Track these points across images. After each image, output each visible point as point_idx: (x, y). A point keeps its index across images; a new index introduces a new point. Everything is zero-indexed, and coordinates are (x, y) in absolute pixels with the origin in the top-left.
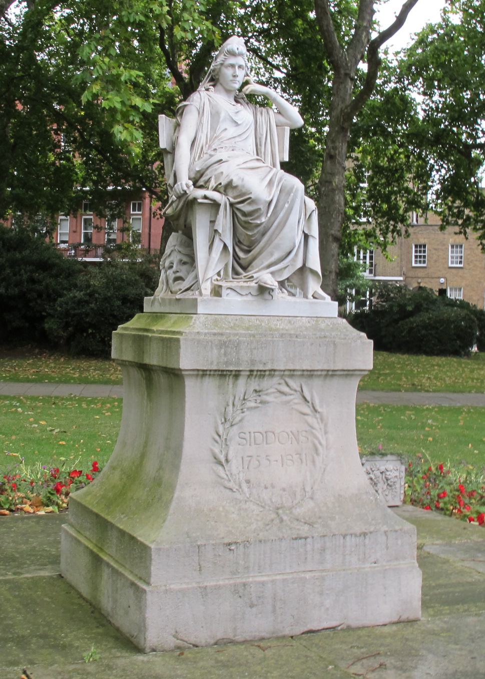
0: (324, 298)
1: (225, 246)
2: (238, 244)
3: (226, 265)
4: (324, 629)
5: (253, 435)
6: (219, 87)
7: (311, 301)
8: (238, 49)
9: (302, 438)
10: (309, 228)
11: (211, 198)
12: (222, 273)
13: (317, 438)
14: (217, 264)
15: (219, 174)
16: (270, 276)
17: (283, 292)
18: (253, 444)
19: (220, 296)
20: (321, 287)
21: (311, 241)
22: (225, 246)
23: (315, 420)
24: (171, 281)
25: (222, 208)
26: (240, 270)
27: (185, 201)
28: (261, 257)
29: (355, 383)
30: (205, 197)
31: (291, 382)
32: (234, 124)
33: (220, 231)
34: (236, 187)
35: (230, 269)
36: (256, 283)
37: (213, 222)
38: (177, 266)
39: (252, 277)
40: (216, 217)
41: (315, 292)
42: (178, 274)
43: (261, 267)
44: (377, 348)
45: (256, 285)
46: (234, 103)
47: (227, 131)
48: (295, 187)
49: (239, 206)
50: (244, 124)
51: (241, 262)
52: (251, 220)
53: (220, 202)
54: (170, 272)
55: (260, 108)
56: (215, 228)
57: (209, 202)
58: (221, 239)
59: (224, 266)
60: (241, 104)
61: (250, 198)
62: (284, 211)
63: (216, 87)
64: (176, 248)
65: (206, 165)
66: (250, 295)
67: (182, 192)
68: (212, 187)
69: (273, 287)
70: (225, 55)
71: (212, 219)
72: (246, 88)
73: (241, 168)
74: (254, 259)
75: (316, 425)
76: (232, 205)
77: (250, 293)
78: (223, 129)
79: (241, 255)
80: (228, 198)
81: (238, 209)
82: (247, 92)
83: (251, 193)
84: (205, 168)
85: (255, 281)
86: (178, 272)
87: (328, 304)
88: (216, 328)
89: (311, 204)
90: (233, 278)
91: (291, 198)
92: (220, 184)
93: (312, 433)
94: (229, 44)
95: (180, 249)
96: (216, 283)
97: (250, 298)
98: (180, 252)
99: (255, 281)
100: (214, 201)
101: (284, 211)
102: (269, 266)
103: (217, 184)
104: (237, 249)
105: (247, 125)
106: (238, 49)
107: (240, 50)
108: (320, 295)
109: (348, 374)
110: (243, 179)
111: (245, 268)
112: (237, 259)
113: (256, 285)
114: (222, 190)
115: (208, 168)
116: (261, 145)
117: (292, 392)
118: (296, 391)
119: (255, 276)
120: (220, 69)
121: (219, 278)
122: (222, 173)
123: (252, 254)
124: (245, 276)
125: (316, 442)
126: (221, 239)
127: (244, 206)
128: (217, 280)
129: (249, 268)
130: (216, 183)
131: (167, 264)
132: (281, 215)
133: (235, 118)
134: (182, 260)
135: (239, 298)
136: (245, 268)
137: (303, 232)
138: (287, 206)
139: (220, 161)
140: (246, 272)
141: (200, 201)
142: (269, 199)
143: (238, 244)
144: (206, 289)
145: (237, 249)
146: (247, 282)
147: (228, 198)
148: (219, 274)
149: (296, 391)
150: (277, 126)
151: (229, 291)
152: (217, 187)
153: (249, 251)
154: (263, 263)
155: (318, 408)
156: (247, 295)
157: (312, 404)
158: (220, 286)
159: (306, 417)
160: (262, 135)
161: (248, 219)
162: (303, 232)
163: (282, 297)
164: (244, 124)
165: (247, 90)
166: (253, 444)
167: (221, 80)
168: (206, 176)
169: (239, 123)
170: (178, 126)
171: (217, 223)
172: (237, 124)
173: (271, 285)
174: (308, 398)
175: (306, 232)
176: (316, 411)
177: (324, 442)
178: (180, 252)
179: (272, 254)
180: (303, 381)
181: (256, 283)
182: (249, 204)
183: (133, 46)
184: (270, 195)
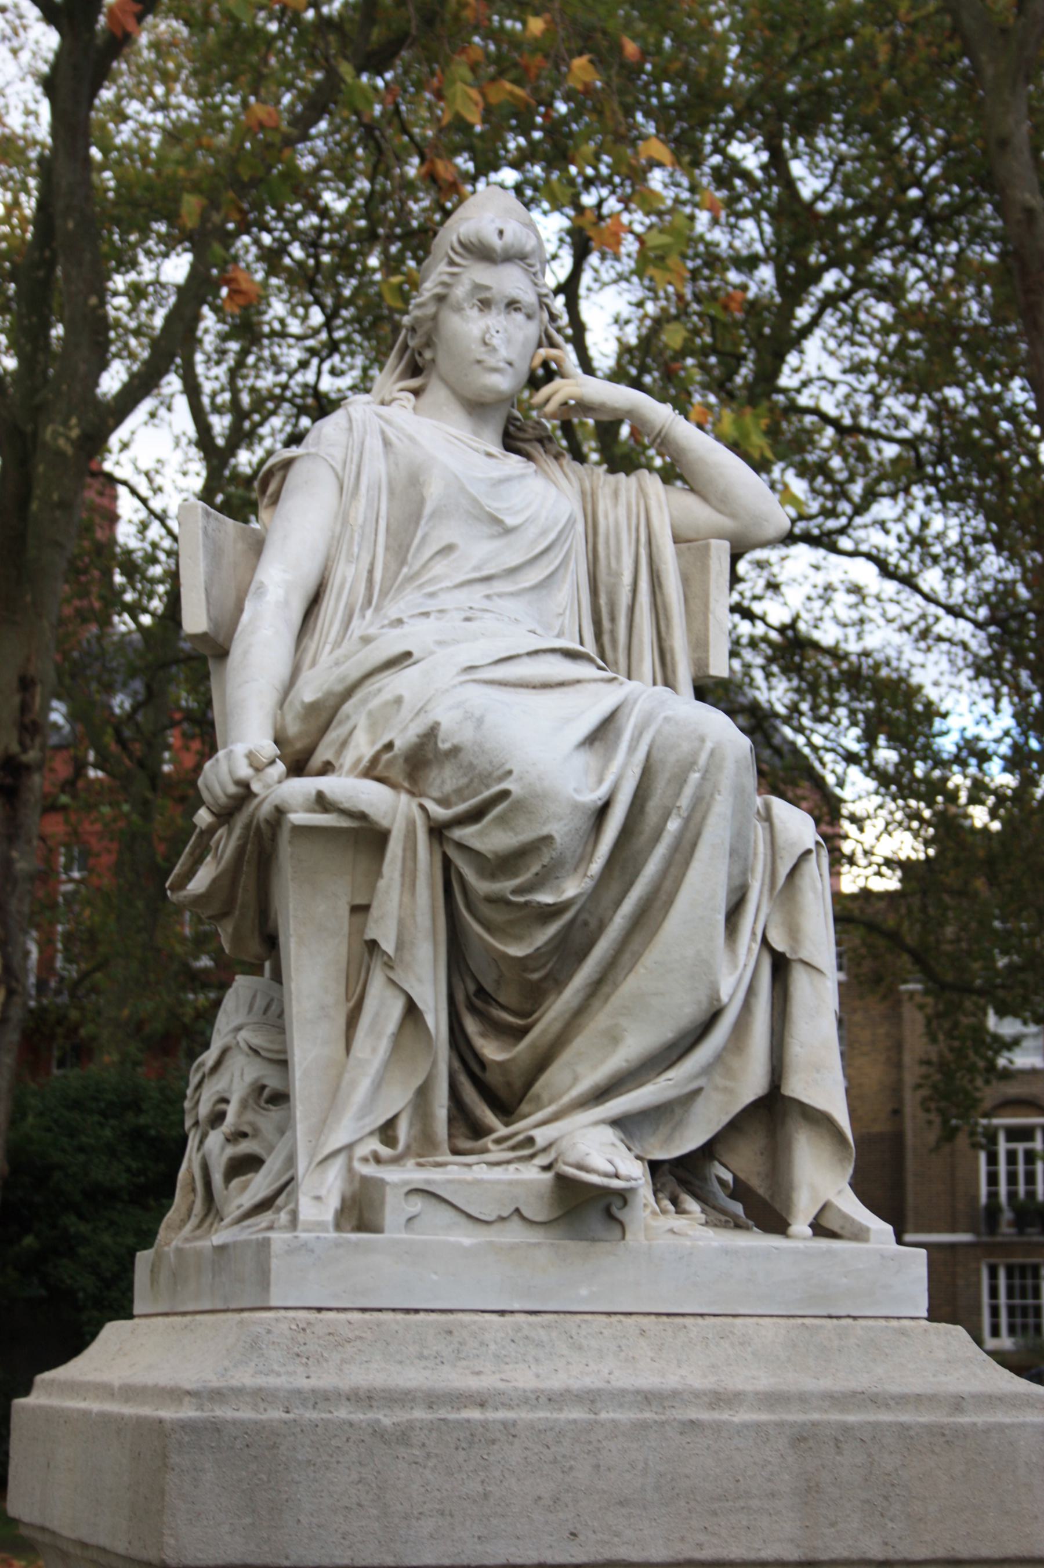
0: (860, 1234)
1: (412, 1010)
2: (478, 1003)
3: (423, 1093)
6: (437, 393)
7: (800, 1244)
8: (501, 233)
10: (793, 932)
11: (346, 805)
12: (403, 1131)
14: (378, 1085)
15: (386, 704)
16: (610, 1134)
17: (680, 1211)
19: (377, 1229)
20: (851, 1185)
21: (800, 982)
22: (412, 1010)
24: (217, 1178)
25: (395, 848)
26: (489, 1117)
27: (247, 827)
28: (566, 1056)
30: (322, 802)
33: (388, 946)
34: (455, 751)
35: (441, 1110)
36: (547, 1168)
37: (360, 910)
38: (240, 1114)
39: (530, 1141)
40: (372, 888)
41: (825, 1207)
42: (245, 1147)
43: (566, 1099)
44: (125, 1312)
45: (548, 1176)
46: (497, 450)
47: (454, 556)
48: (709, 745)
49: (464, 834)
50: (532, 531)
51: (492, 1078)
52: (514, 892)
53: (385, 823)
54: (215, 1138)
55: (612, 478)
56: (370, 935)
57: (344, 823)
58: (392, 982)
59: (409, 1094)
60: (529, 457)
61: (505, 794)
62: (661, 850)
63: (427, 398)
64: (243, 1035)
65: (341, 680)
66: (516, 1223)
67: (232, 789)
68: (359, 760)
69: (633, 1184)
70: (452, 263)
71: (360, 901)
73: (475, 681)
74: (543, 1061)
76: (438, 831)
77: (517, 1210)
78: (443, 544)
79: (492, 1051)
80: (422, 807)
81: (461, 847)
83: (510, 773)
84: (339, 688)
85: (542, 1160)
86: (244, 1135)
90: (455, 1152)
91: (688, 791)
92: (389, 746)
94: (467, 219)
95: (257, 1041)
96: (369, 1170)
97: (515, 1234)
98: (256, 1052)
99: (542, 1160)
100: (362, 816)
101: (661, 850)
102: (601, 1094)
103: (378, 746)
104: (471, 1026)
105: (544, 533)
106: (501, 233)
107: (508, 236)
108: (845, 1217)
110: (480, 722)
111: (507, 1110)
112: (476, 1068)
113: (548, 1176)
114: (397, 774)
115: (349, 693)
116: (613, 619)
119: (542, 1135)
120: (434, 318)
121: (385, 1151)
122: (398, 701)
123: (533, 1046)
124: (498, 1141)
126: (392, 982)
127: (481, 834)
128: (378, 1159)
129: (524, 1108)
130: (373, 743)
131: (204, 1110)
132: (652, 868)
133: (492, 505)
134: (263, 1087)
135: (466, 1237)
136: (507, 1110)
137: (765, 942)
138: (673, 825)
139: (403, 659)
140: (507, 1124)
141: (298, 818)
142: (594, 796)
143: (478, 1003)
144: (318, 1198)
145: (471, 1026)
146: (508, 1162)
147: (422, 807)
148: (387, 1132)
150: (677, 540)
151: (417, 1205)
152: (375, 760)
153: (522, 1032)
154: (576, 1080)
156: (502, 1219)
158: (381, 1183)
160: (618, 575)
161: (505, 886)
162: (765, 942)
163: (672, 1231)
164: (532, 531)
165: (547, 400)
167: (444, 364)
168: (340, 723)
169: (510, 521)
170: (257, 546)
171: (374, 912)
172: (501, 529)
173: (607, 1175)
175: (779, 944)
178: (256, 1052)
179: (613, 1038)
181: (547, 1168)
182: (502, 821)
184: (600, 781)
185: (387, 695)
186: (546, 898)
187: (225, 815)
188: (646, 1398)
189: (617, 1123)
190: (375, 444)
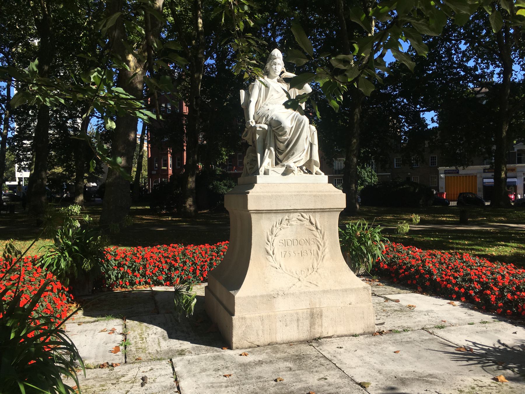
4: (324, 337)
5: (286, 241)
9: (312, 242)
13: (319, 242)
18: (286, 245)
23: (317, 233)
29: (337, 215)
30: (260, 127)
31: (304, 214)
32: (277, 92)
72: (283, 74)
75: (318, 236)
82: (283, 77)
87: (323, 177)
88: (103, 21)
89: (313, 128)
93: (316, 239)
109: (331, 210)
111: (281, 161)
117: (306, 220)
118: (307, 219)
125: (319, 244)
149: (307, 219)
155: (319, 227)
157: (316, 225)
159: (313, 232)
166: (286, 245)
174: (314, 223)
176: (423, 329)
177: (322, 244)
180: (311, 214)
183: (413, 39)
186: (286, 138)
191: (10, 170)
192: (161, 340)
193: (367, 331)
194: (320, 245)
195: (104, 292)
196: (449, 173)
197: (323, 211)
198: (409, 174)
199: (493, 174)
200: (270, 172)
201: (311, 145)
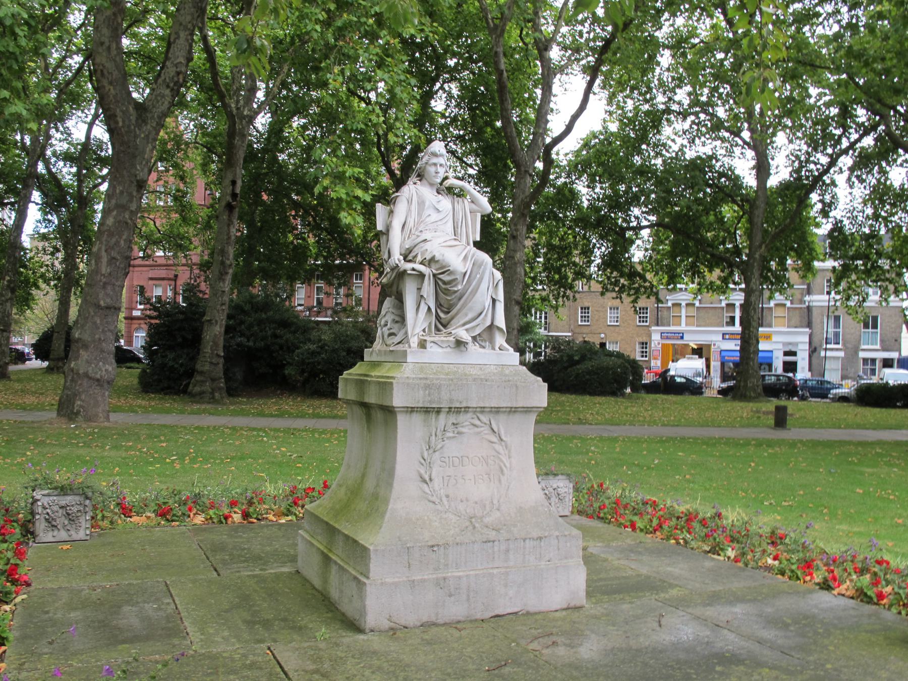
0: (508, 350)
1: (429, 309)
3: (430, 324)
6: (424, 181)
9: (490, 462)
10: (496, 294)
13: (502, 462)
21: (498, 304)
22: (429, 309)
24: (386, 336)
25: (426, 278)
29: (533, 417)
30: (413, 269)
31: (482, 417)
34: (438, 261)
37: (419, 289)
42: (391, 331)
47: (787, 349)
49: (440, 276)
51: (442, 321)
74: (452, 318)
75: (501, 451)
76: (434, 275)
79: (442, 315)
81: (440, 279)
97: (449, 350)
102: (464, 325)
104: (439, 311)
109: (527, 410)
111: (445, 326)
114: (427, 264)
119: (453, 332)
131: (383, 323)
132: (474, 283)
135: (440, 350)
136: (445, 326)
139: (425, 240)
142: (464, 271)
145: (439, 311)
151: (432, 344)
153: (448, 313)
158: (425, 341)
161: (448, 286)
167: (426, 176)
170: (391, 212)
172: (438, 211)
174: (496, 430)
177: (508, 465)
179: (466, 315)
180: (491, 416)
182: (449, 275)
185: (424, 248)
186: (456, 289)
187: (392, 269)
188: (27, 96)
189: (467, 330)
190: (415, 194)
191: (769, 193)
192: (352, 223)
193: (572, 605)
194: (504, 468)
195: (318, 294)
196: (667, 338)
197: (513, 411)
198: (603, 335)
199: (739, 342)
200: (428, 345)
201: (494, 301)
